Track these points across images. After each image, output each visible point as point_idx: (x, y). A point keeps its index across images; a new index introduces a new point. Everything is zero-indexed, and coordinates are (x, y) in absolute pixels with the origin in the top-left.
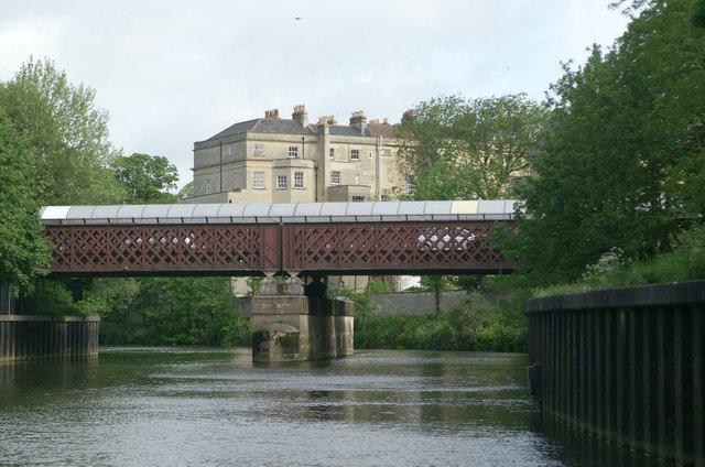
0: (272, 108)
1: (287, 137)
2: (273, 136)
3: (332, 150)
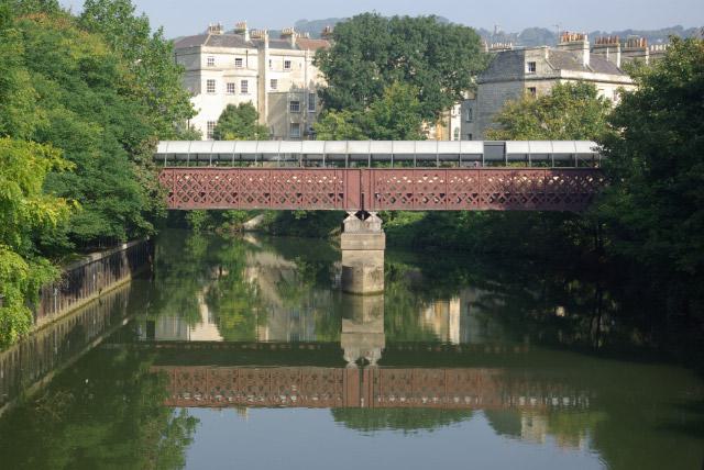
1: (234, 50)
2: (222, 49)
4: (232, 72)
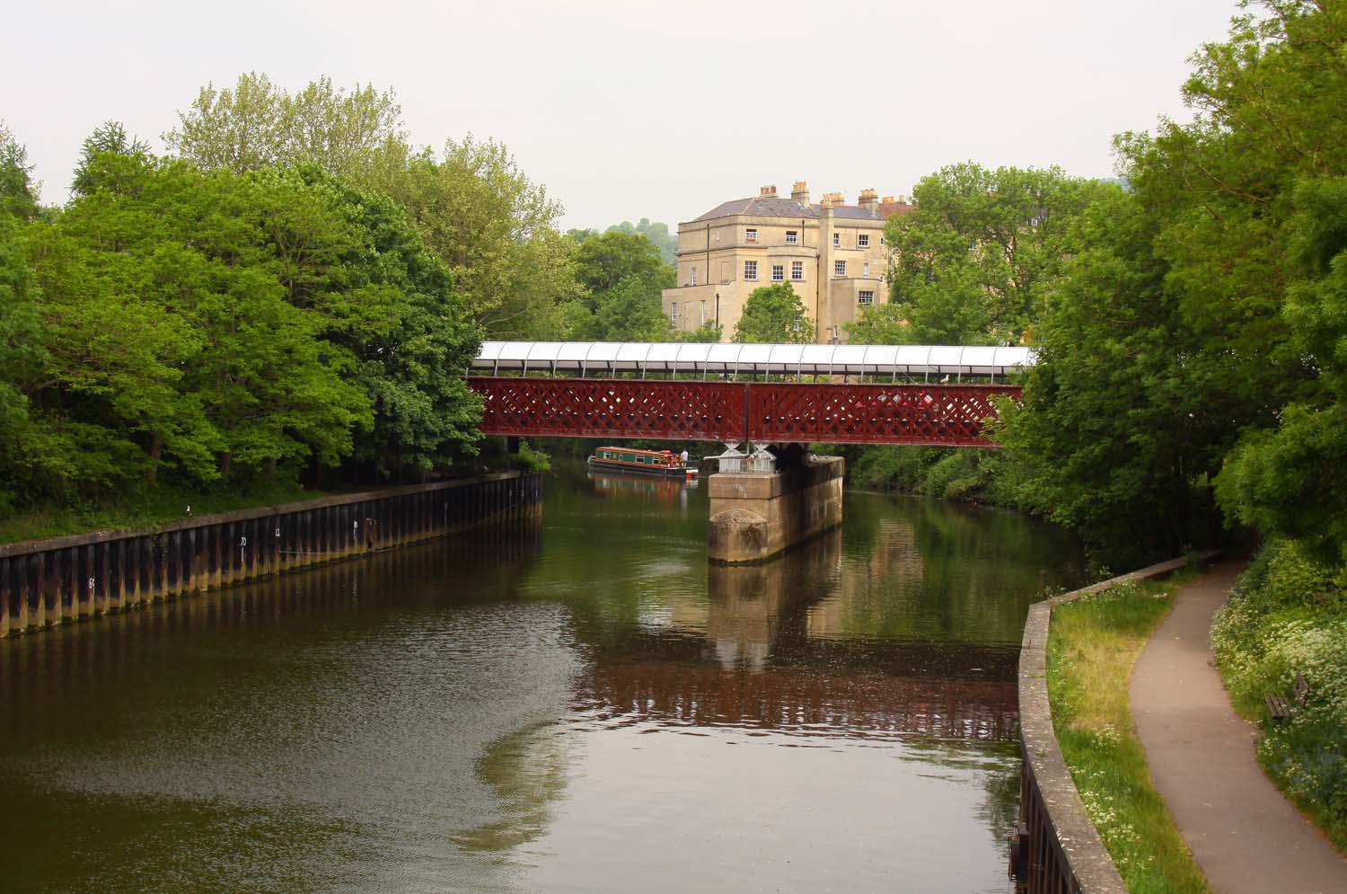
0: (769, 184)
1: (785, 221)
3: (837, 235)
4: (782, 251)
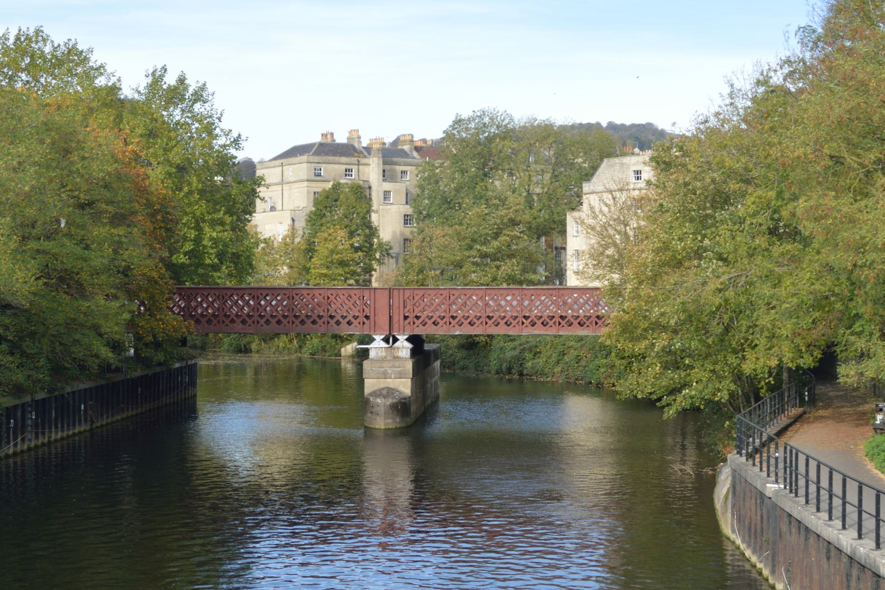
1: (344, 159)
3: (384, 171)
